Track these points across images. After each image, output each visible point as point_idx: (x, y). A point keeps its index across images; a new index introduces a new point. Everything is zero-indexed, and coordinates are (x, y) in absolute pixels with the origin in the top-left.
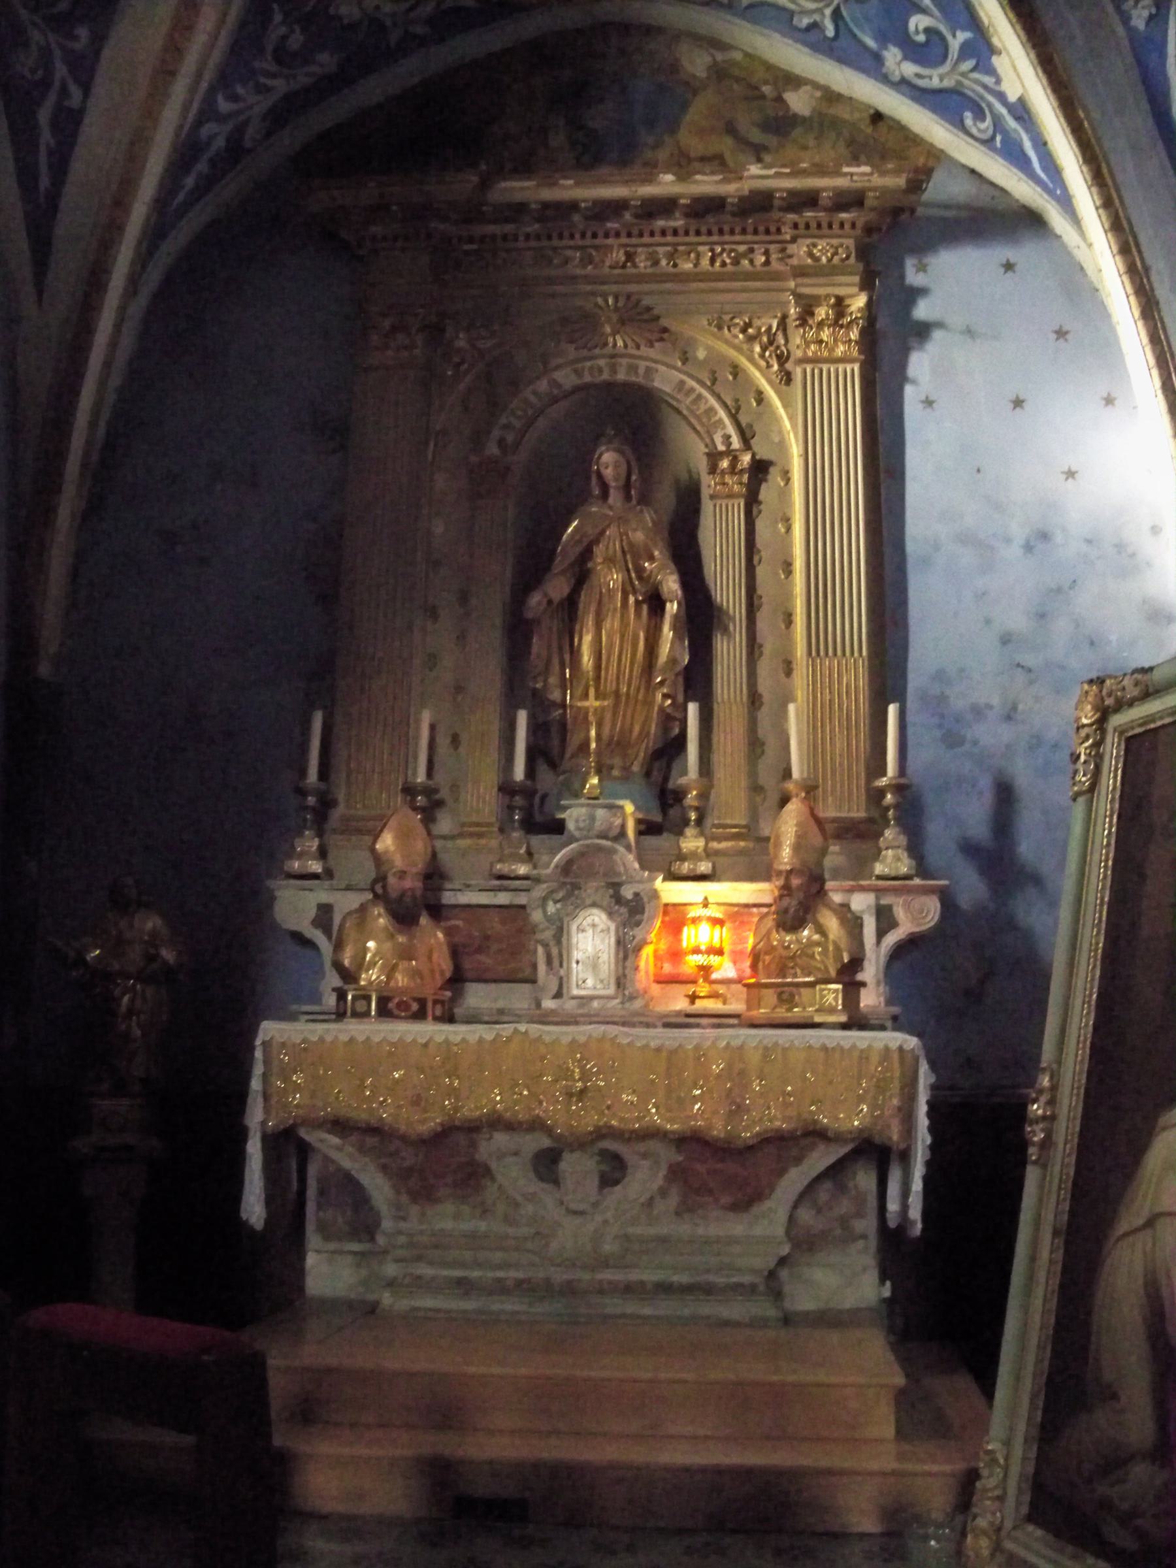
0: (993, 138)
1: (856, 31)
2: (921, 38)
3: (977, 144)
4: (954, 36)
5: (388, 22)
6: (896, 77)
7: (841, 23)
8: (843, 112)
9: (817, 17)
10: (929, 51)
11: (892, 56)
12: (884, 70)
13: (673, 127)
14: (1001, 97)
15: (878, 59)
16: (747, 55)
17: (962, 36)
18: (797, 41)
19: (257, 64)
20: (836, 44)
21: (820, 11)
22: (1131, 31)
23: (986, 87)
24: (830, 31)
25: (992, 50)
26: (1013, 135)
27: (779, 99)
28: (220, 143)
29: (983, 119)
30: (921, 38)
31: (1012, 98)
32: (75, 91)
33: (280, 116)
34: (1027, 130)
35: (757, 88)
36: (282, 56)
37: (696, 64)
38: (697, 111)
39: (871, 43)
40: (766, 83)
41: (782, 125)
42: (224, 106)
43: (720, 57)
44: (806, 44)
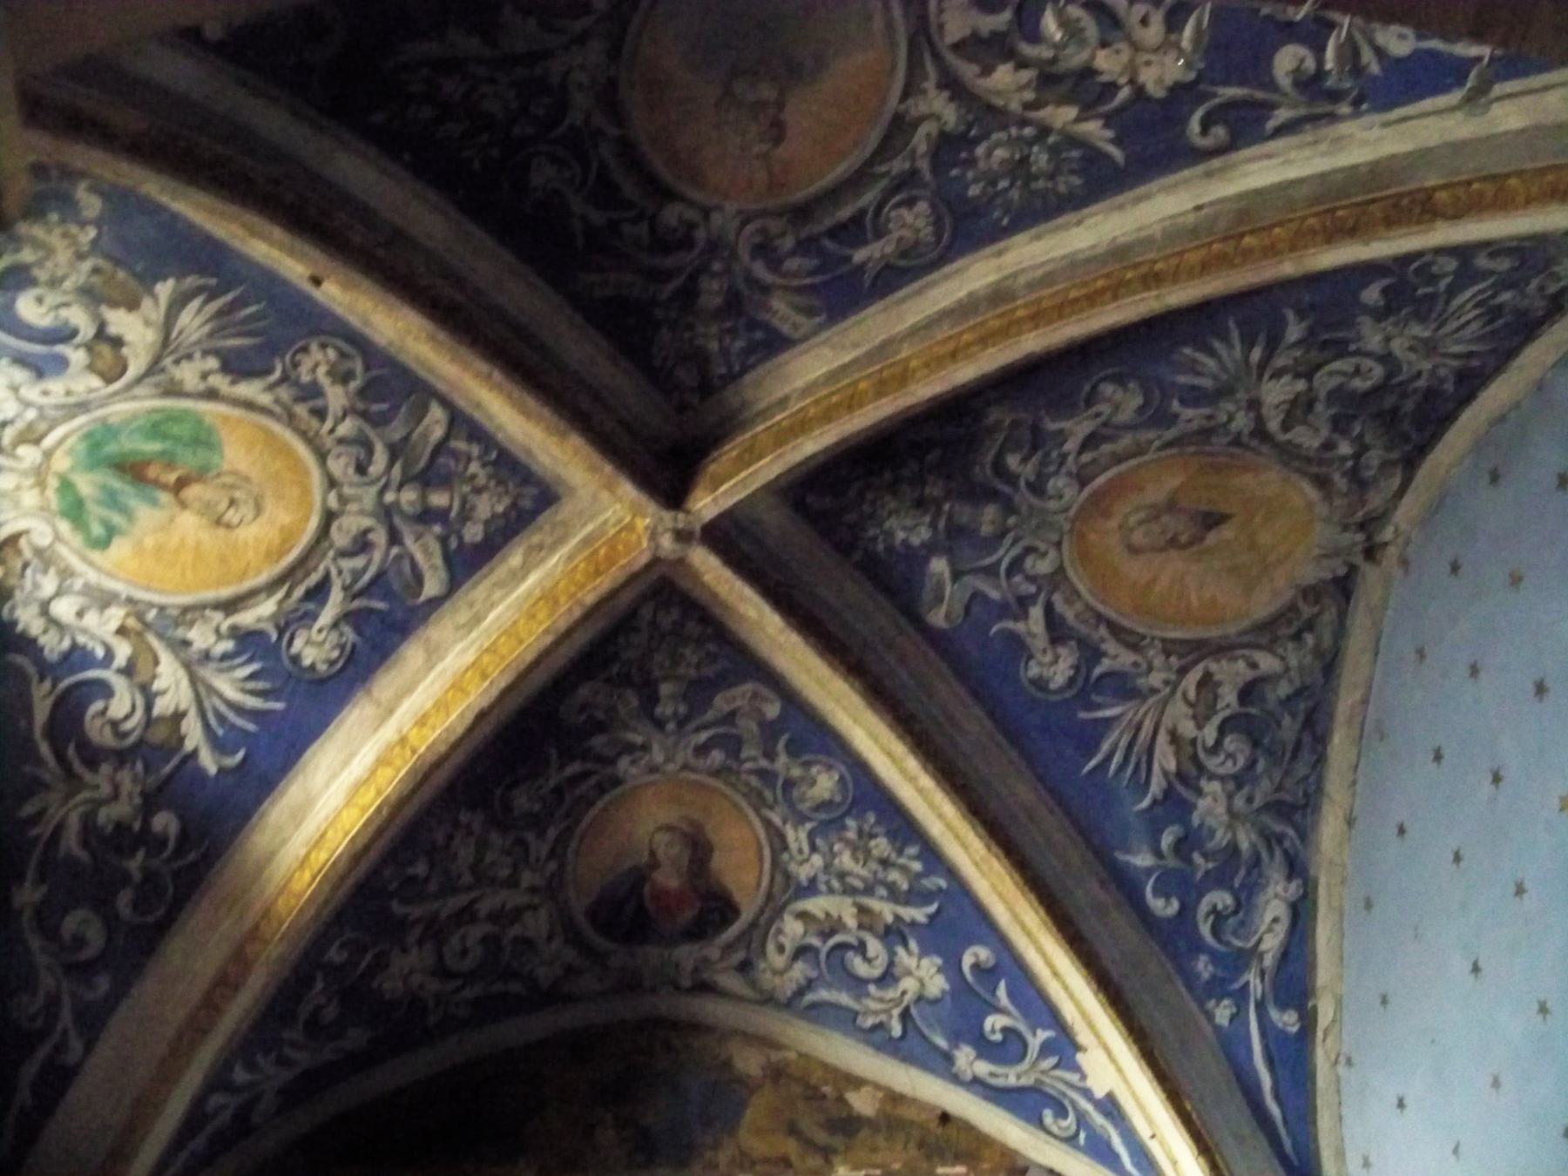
0: (1077, 1134)
1: (926, 1031)
2: (998, 1037)
3: (1056, 1143)
4: (1034, 1034)
5: (431, 1004)
6: (968, 1076)
7: (910, 1025)
8: (909, 1113)
9: (883, 1017)
10: (1008, 1049)
11: (965, 1058)
12: (954, 1070)
13: (731, 1127)
14: (1087, 1093)
15: (948, 1058)
16: (800, 1055)
17: (1043, 1035)
18: (858, 1041)
19: (286, 1035)
20: (903, 1044)
21: (887, 1011)
22: (1217, 1029)
23: (1067, 1084)
24: (897, 1030)
25: (1077, 1048)
26: (1099, 1130)
27: (841, 1099)
28: (225, 1117)
29: (1065, 1115)
30: (998, 1037)
31: (1099, 1093)
32: (76, 1045)
33: (296, 1094)
34: (1116, 1126)
35: (816, 1088)
36: (314, 1027)
37: (749, 1062)
38: (756, 1112)
39: (941, 1042)
40: (826, 1083)
41: (847, 1125)
42: (240, 1075)
43: (775, 1056)
44: (868, 1043)
